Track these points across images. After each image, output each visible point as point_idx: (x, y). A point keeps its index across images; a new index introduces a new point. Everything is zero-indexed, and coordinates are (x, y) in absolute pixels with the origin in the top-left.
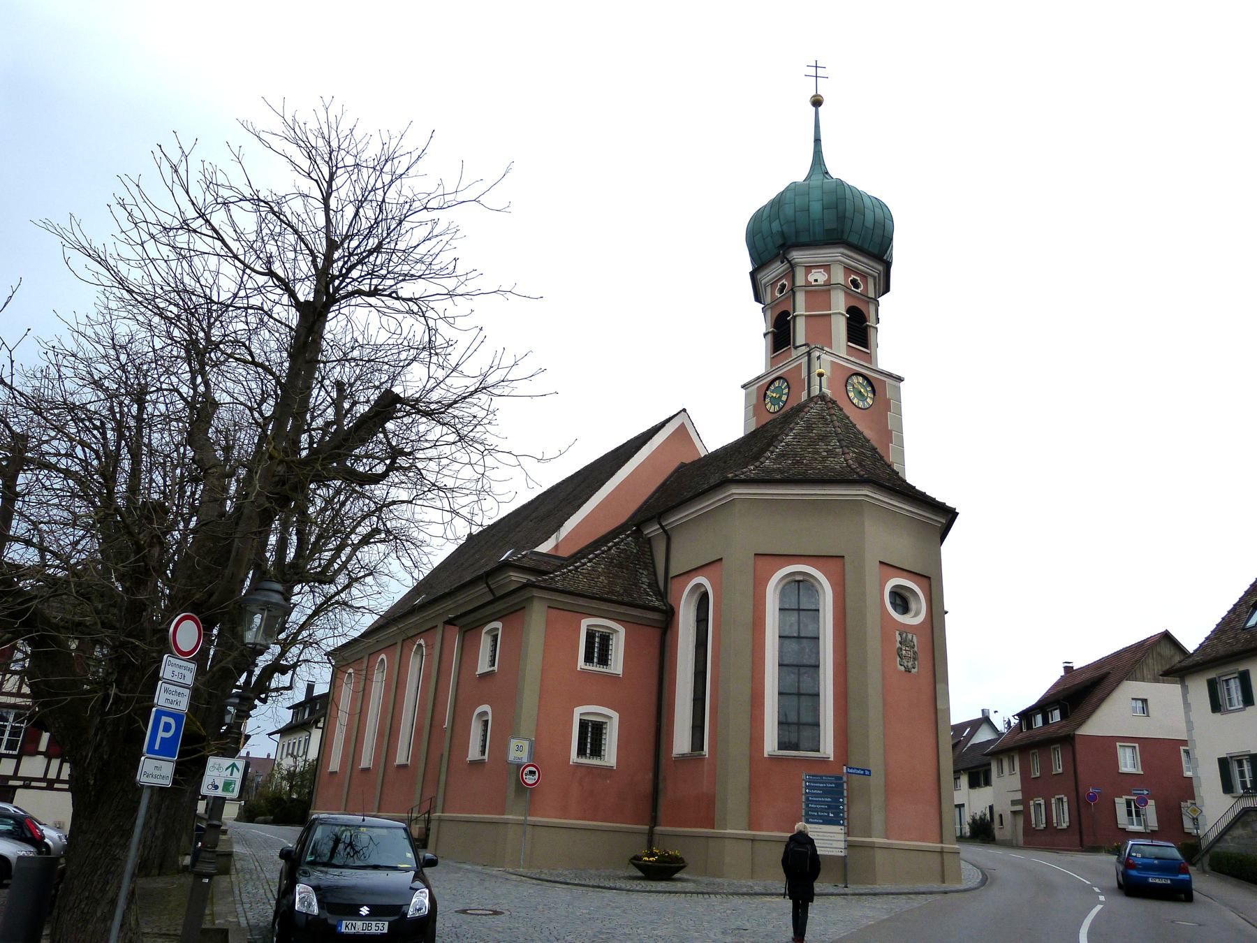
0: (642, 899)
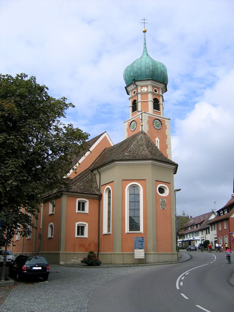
0: (91, 269)
